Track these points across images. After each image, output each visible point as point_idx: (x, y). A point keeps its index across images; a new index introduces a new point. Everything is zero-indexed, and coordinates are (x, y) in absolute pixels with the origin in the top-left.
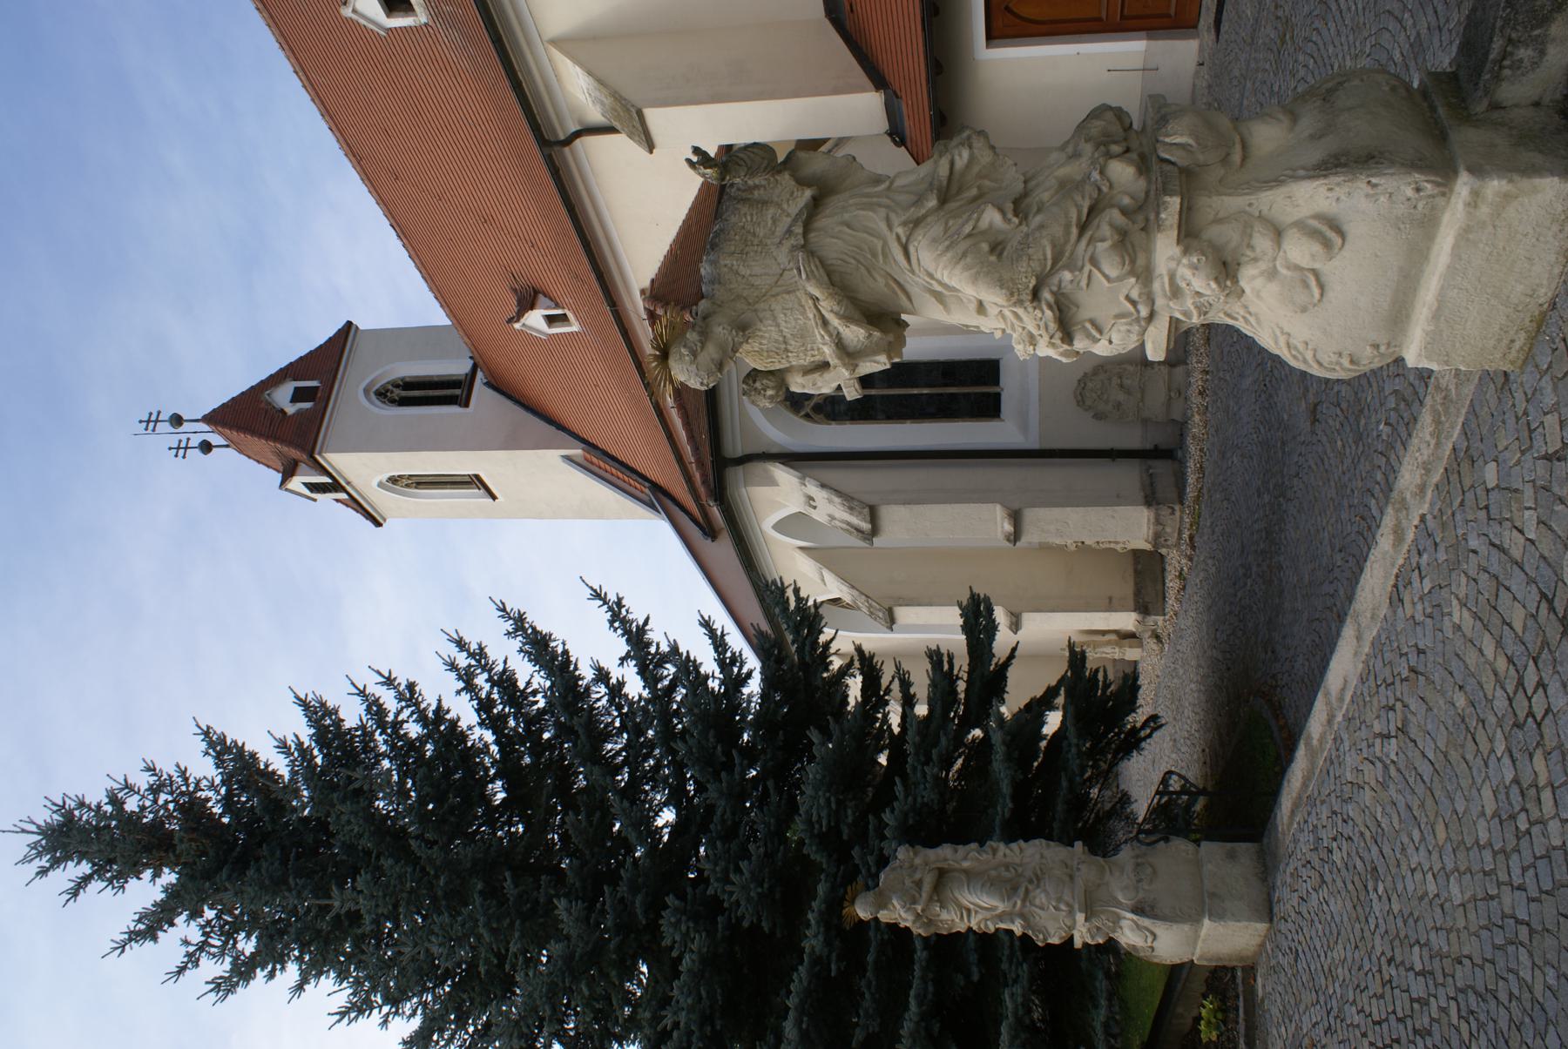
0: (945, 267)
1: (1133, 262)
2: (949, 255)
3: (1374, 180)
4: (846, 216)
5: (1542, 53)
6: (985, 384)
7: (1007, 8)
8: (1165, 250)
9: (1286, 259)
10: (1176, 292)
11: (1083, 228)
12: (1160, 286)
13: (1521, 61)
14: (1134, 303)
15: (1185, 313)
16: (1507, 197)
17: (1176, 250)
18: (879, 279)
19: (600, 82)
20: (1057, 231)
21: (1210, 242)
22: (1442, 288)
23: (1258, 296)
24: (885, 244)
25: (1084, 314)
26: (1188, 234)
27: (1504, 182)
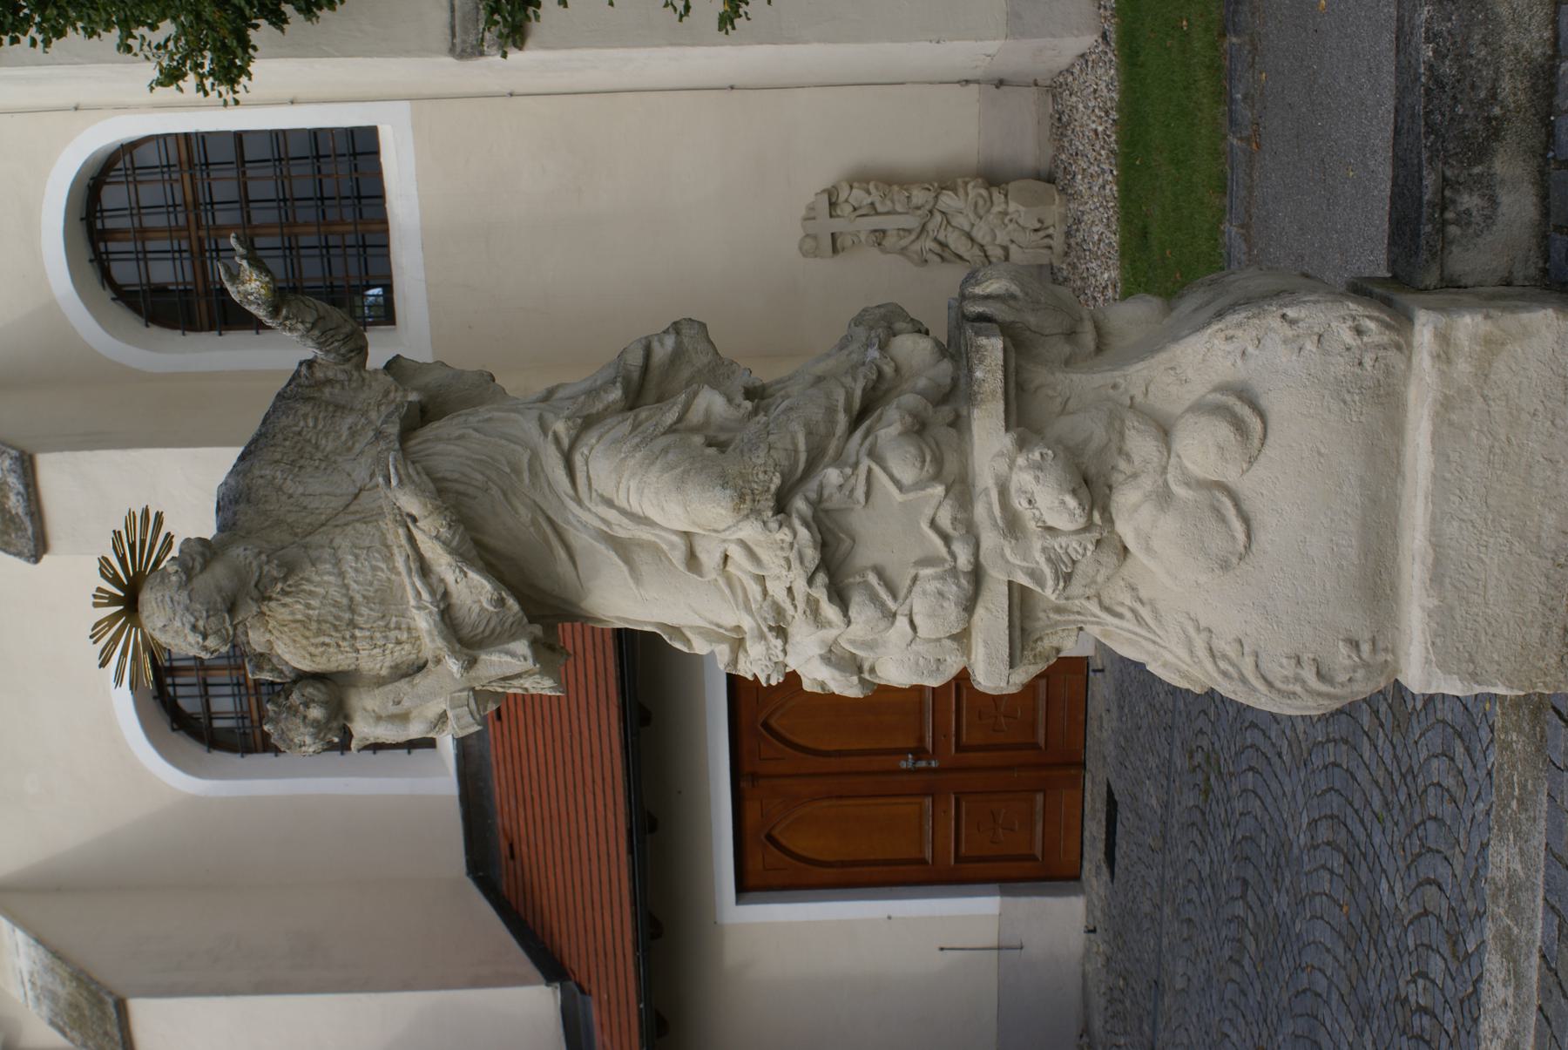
0: (633, 475)
1: (939, 462)
2: (638, 455)
3: (1291, 313)
5: (1493, 201)
7: (771, 838)
8: (988, 435)
9: (1183, 470)
10: (1012, 525)
11: (855, 424)
12: (985, 510)
13: (1468, 212)
14: (946, 539)
15: (1033, 574)
16: (1491, 345)
17: (1006, 441)
18: (522, 511)
19: (56, 954)
21: (1059, 441)
22: (1433, 519)
23: (1148, 550)
24: (535, 456)
25: (867, 554)
26: (1022, 419)
27: (1479, 318)
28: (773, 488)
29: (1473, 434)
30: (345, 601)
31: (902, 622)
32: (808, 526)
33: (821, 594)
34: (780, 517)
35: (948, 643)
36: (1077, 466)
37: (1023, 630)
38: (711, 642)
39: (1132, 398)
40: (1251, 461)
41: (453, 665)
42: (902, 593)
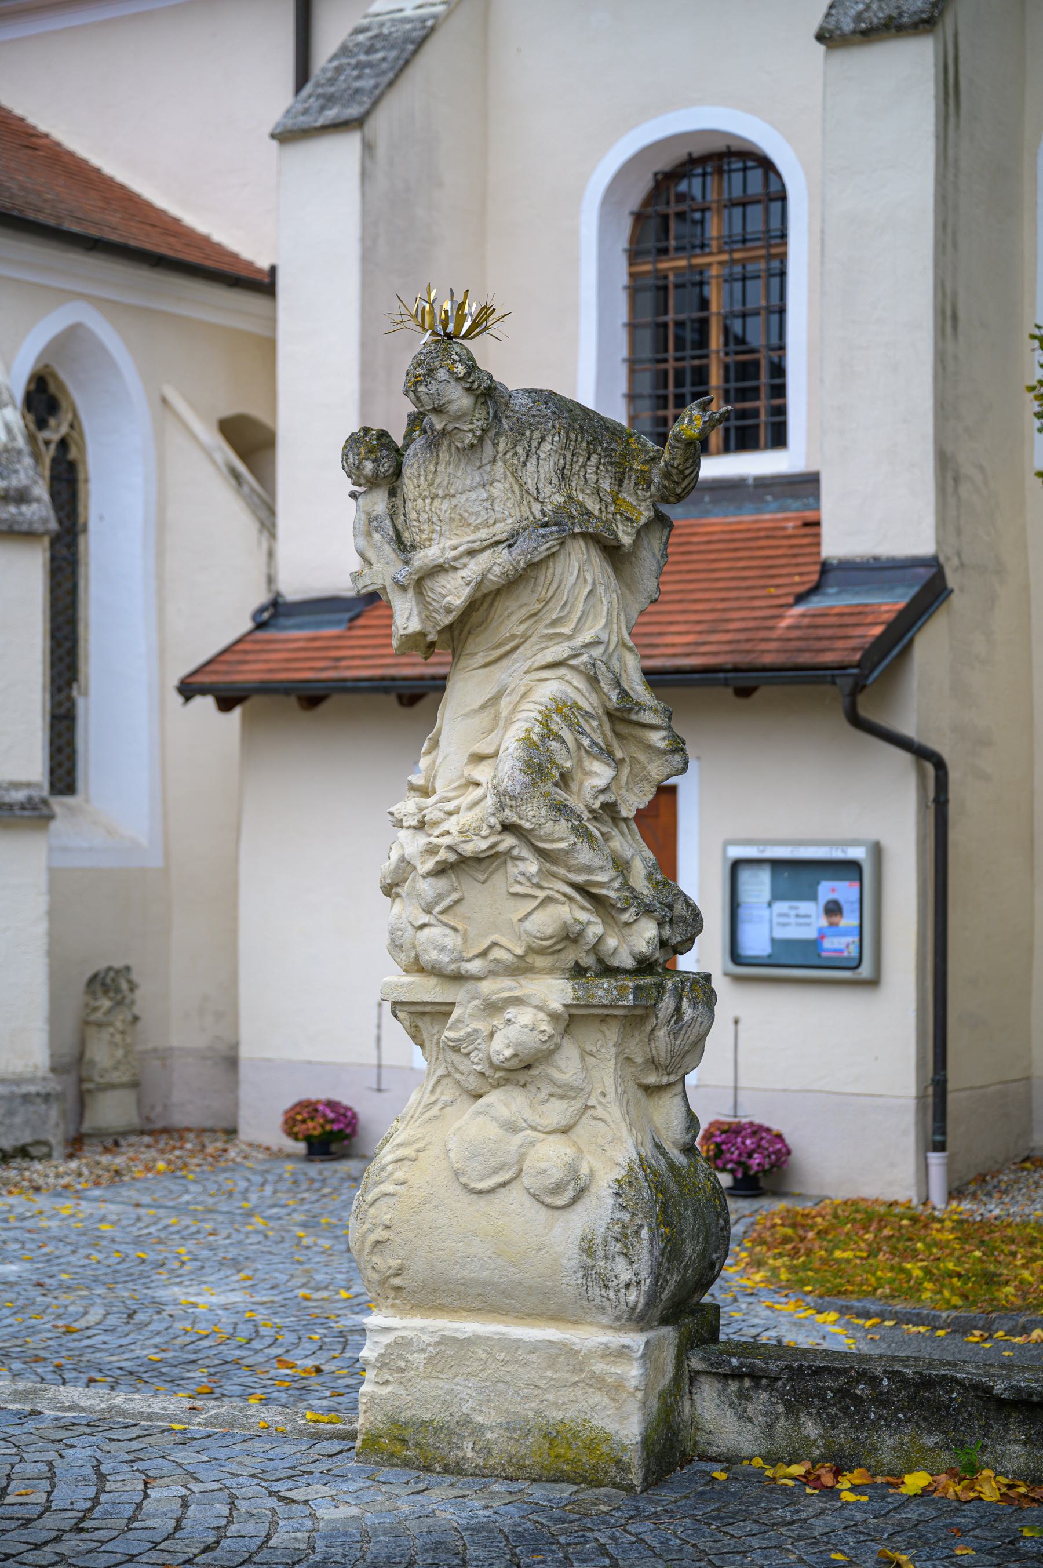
4: (601, 589)
9: (532, 1144)
10: (493, 1007)
12: (493, 988)
14: (484, 954)
18: (523, 627)
21: (558, 1047)
22: (489, 1339)
28: (522, 823)
29: (549, 1373)
30: (452, 491)
31: (425, 918)
32: (491, 847)
33: (443, 855)
34: (499, 827)
35: (413, 954)
36: (537, 1060)
37: (424, 1014)
38: (427, 770)
39: (593, 1107)
40: (535, 1196)
41: (403, 573)
42: (442, 918)
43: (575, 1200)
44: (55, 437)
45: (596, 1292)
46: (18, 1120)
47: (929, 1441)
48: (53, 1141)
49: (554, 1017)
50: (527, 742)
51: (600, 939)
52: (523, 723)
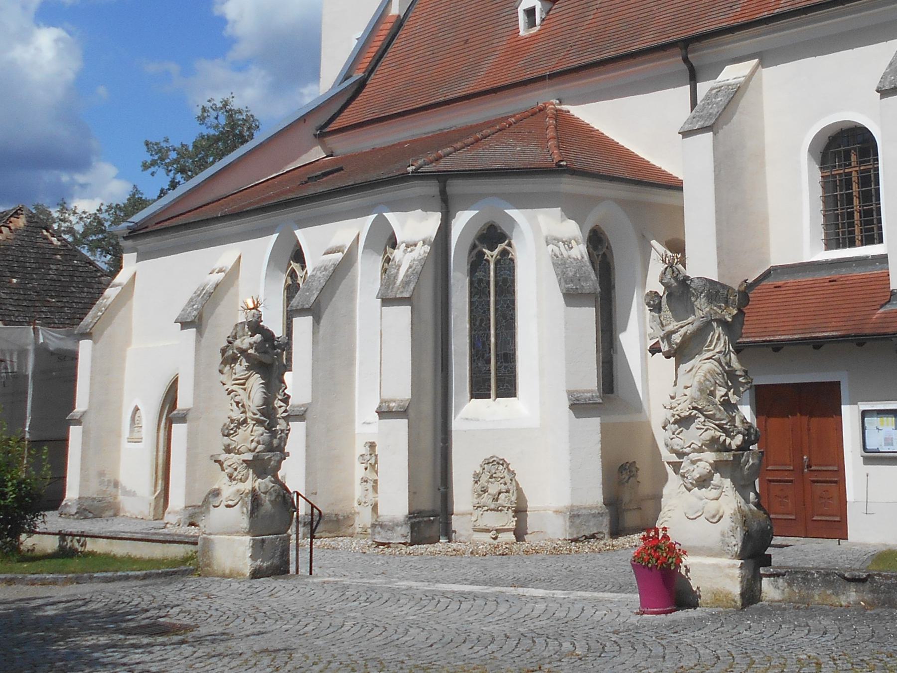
6: (497, 387)
8: (710, 456)
10: (693, 462)
12: (694, 456)
14: (689, 447)
20: (718, 416)
41: (662, 334)
43: (719, 520)
44: (601, 253)
45: (726, 548)
46: (591, 524)
47: (829, 592)
48: (605, 532)
49: (711, 464)
50: (700, 383)
51: (725, 440)
52: (700, 376)
